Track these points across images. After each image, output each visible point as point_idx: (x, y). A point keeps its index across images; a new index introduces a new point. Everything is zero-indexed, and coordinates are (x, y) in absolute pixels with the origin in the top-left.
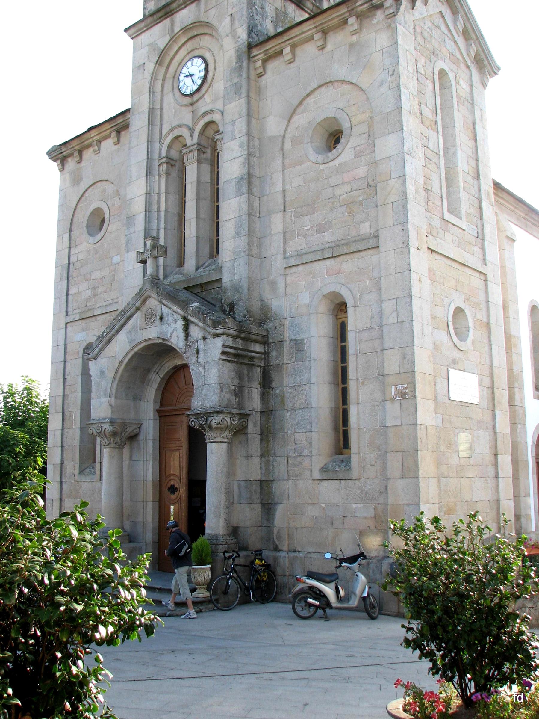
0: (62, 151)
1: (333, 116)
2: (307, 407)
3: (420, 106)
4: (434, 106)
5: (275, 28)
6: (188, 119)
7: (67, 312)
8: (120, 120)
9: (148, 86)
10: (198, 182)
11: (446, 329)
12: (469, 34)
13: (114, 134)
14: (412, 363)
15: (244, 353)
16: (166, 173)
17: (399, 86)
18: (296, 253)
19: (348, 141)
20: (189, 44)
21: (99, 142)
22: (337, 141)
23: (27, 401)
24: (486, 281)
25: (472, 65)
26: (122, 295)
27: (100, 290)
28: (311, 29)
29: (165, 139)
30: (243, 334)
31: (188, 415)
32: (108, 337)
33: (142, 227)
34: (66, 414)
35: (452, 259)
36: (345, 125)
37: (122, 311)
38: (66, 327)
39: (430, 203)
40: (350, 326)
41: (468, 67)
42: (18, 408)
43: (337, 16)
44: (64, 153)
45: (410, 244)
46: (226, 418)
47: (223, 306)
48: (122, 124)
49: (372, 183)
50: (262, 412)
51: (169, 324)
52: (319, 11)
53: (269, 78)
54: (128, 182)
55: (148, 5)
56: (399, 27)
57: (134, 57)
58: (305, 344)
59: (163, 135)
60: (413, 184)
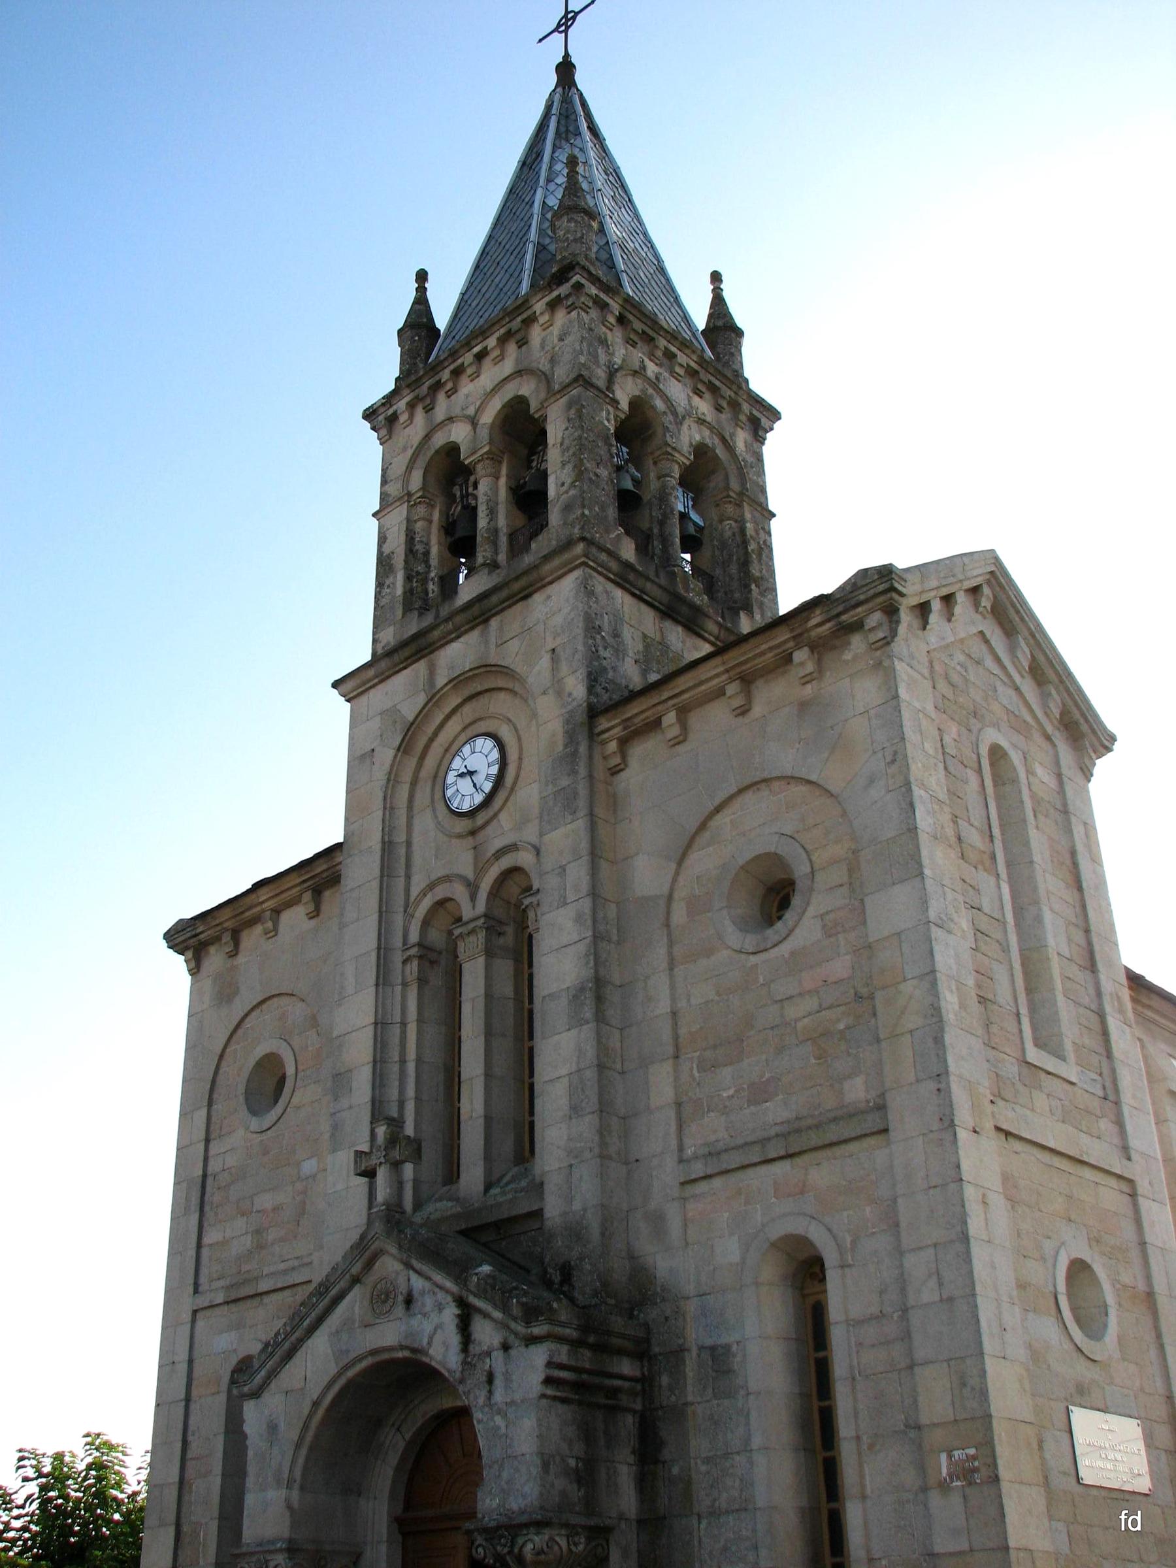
0: (198, 931)
1: (773, 850)
2: (744, 1507)
3: (955, 823)
4: (985, 820)
5: (644, 673)
6: (465, 865)
7: (196, 1285)
8: (321, 867)
9: (381, 795)
10: (489, 996)
11: (1053, 1311)
12: (1043, 673)
13: (307, 896)
14: (983, 1394)
15: (597, 1380)
16: (419, 979)
17: (907, 784)
18: (706, 1150)
19: (808, 904)
20: (467, 709)
21: (277, 912)
22: (784, 904)
23: (95, 1496)
24: (1133, 1195)
25: (1057, 733)
26: (322, 1247)
27: (272, 1235)
28: (717, 676)
29: (417, 906)
30: (592, 1336)
31: (469, 1532)
32: (287, 1345)
33: (367, 1098)
34: (185, 1529)
35: (1051, 1150)
36: (800, 870)
37: (320, 1285)
38: (194, 1321)
39: (994, 1029)
40: (835, 1312)
41: (1048, 738)
42: (71, 1514)
43: (771, 649)
44: (202, 936)
45: (956, 1122)
46: (557, 1539)
47: (546, 1272)
48: (324, 875)
49: (864, 991)
50: (639, 1522)
51: (424, 1315)
52: (732, 638)
53: (633, 778)
54: (336, 997)
55: (381, 635)
56: (898, 665)
57: (351, 738)
58: (734, 1356)
59: (412, 899)
60: (954, 988)
